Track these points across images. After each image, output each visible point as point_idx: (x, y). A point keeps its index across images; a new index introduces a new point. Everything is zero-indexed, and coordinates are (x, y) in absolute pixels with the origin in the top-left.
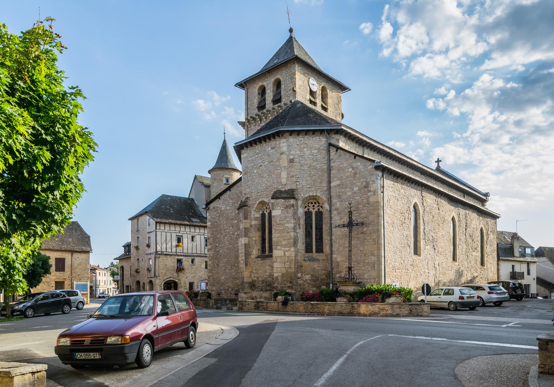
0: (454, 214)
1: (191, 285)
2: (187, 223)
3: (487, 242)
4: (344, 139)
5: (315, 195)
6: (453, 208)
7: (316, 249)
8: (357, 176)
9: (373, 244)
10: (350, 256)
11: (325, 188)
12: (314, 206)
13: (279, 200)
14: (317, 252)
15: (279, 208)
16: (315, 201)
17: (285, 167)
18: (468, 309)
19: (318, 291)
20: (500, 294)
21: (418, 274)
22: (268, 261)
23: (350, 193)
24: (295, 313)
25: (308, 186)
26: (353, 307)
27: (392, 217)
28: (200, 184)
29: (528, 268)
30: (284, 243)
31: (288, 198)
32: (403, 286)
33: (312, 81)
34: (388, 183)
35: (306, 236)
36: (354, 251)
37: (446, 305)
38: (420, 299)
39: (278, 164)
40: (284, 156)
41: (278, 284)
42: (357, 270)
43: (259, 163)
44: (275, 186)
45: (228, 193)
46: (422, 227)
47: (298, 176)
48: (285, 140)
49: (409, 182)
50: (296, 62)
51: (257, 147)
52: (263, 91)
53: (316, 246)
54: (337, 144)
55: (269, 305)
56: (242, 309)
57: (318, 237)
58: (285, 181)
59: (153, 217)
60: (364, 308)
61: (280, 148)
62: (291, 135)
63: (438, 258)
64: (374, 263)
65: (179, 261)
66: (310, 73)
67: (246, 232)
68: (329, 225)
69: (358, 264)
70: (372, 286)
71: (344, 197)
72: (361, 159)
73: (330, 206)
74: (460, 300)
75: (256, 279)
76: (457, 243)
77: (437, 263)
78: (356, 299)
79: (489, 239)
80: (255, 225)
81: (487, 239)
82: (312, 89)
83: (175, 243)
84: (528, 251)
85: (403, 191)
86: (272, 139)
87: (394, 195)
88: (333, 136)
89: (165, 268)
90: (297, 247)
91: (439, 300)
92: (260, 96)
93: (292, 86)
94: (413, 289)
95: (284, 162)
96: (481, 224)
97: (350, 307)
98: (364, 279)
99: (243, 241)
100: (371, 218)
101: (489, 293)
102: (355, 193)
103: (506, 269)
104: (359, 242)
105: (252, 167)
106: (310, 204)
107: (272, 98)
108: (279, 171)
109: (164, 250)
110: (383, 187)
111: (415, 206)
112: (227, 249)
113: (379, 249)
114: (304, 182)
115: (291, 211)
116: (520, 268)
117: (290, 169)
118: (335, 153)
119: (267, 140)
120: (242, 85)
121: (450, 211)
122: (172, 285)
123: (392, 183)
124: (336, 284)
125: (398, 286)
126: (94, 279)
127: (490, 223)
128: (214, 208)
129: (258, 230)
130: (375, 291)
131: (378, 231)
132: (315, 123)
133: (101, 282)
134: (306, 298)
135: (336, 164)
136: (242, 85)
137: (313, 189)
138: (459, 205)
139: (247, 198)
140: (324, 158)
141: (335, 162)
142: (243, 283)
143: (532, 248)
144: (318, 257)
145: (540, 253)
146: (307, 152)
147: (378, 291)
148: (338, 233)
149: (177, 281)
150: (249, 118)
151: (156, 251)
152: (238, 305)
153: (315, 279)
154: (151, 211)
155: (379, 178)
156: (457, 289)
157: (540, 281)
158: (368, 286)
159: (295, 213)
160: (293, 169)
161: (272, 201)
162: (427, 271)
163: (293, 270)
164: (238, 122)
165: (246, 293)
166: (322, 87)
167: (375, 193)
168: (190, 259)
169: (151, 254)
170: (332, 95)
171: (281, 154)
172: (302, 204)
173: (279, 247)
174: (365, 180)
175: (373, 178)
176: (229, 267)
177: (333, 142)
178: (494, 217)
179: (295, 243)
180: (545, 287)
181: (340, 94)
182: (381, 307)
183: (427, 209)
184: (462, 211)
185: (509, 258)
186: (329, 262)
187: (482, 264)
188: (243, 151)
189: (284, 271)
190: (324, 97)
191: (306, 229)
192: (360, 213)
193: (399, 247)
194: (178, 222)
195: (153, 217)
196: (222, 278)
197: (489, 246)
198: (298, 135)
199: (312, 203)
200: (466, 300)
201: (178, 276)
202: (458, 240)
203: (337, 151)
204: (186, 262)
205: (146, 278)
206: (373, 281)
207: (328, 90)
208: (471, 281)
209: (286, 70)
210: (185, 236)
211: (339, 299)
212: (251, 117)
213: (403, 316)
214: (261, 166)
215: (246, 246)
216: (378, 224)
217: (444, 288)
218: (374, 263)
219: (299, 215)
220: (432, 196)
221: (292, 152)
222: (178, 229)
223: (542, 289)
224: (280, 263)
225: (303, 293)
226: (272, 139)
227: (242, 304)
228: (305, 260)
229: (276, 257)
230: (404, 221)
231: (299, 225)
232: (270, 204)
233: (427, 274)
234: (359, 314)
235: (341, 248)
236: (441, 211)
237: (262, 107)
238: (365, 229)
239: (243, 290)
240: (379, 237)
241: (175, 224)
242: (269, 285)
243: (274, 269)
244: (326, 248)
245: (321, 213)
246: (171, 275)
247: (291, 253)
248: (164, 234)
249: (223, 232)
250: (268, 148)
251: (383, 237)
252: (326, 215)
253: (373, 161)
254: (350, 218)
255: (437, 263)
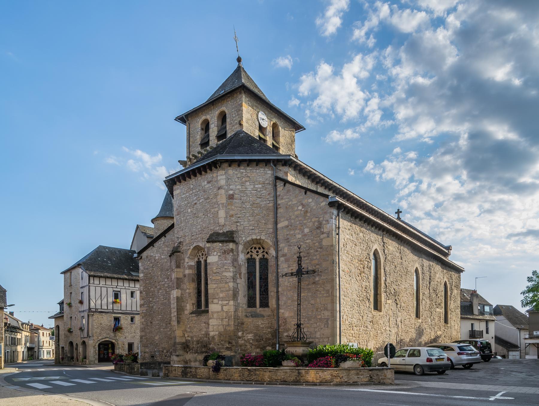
0: (417, 265)
1: (131, 346)
2: (126, 277)
3: (450, 297)
4: (293, 172)
5: (258, 238)
6: (416, 258)
7: (261, 303)
8: (308, 215)
9: (326, 297)
10: (299, 310)
11: (271, 230)
12: (257, 252)
13: (215, 244)
14: (261, 306)
15: (215, 253)
16: (260, 246)
17: (223, 204)
18: (436, 373)
19: (262, 353)
20: (471, 355)
21: (379, 332)
22: (203, 318)
23: (300, 236)
24: (228, 382)
25: (251, 228)
26: (299, 373)
27: (348, 264)
28: (142, 235)
29: (487, 326)
30: (221, 295)
31: (227, 241)
32: (362, 347)
33: (261, 115)
34: (344, 223)
35: (249, 288)
36: (304, 306)
37: (411, 369)
38: (380, 361)
39: (215, 200)
40: (222, 191)
41: (215, 344)
42: (308, 327)
43: (193, 201)
44: (212, 228)
45: (163, 239)
46: (383, 279)
47: (238, 216)
48: (224, 172)
49: (368, 224)
50: (243, 92)
51: (191, 182)
52: (206, 126)
53: (260, 300)
54: (285, 177)
55: (198, 371)
56: (168, 376)
57: (263, 289)
58: (222, 221)
59: (86, 270)
60: (312, 374)
61: (217, 181)
62: (230, 166)
63: (400, 314)
64: (328, 319)
65: (117, 319)
66: (259, 107)
67: (179, 283)
68: (275, 274)
69: (309, 320)
70: (325, 346)
71: (293, 241)
72: (313, 195)
73: (277, 251)
74: (428, 363)
75: (190, 339)
76: (421, 298)
77: (399, 319)
78: (306, 362)
79: (453, 294)
80: (189, 274)
81: (451, 294)
82: (262, 124)
83: (111, 299)
84: (487, 309)
85: (361, 234)
86: (208, 171)
87: (352, 239)
88: (281, 168)
89: (100, 329)
90: (237, 300)
91: (403, 362)
92: (204, 132)
93: (239, 120)
94: (372, 350)
95: (222, 199)
96: (445, 277)
97: (296, 373)
98: (315, 338)
99: (175, 293)
100: (324, 265)
101: (459, 354)
102: (305, 235)
103: (466, 326)
104: (310, 294)
105: (186, 205)
106: (253, 250)
107: (216, 133)
108: (216, 209)
109: (98, 307)
110: (339, 228)
111: (376, 254)
112: (162, 304)
113: (333, 302)
114: (246, 223)
115: (230, 256)
116: (480, 327)
117: (230, 207)
118: (282, 188)
119: (203, 173)
120: (183, 119)
121: (413, 261)
122: (110, 346)
123: (349, 224)
124: (283, 345)
125: (356, 346)
126: (36, 340)
127: (454, 278)
128: (147, 257)
129: (193, 281)
130: (328, 353)
131: (333, 280)
132: (260, 152)
133: (45, 342)
134: (247, 361)
135: (283, 201)
136: (183, 119)
137: (257, 231)
138: (423, 256)
139: (180, 243)
140: (269, 194)
141: (282, 199)
142: (175, 343)
143: (490, 306)
144: (263, 313)
145: (498, 311)
146: (249, 187)
147: (331, 352)
148: (286, 283)
149: (114, 341)
150: (191, 157)
151: (90, 309)
152: (164, 370)
153: (258, 339)
154: (84, 263)
155: (334, 217)
156: (424, 350)
157: (499, 340)
158: (320, 347)
159: (235, 260)
160: (233, 207)
161: (208, 245)
162: (388, 328)
163: (232, 328)
164: (179, 161)
165: (178, 356)
166: (274, 124)
167: (329, 234)
168: (129, 317)
169: (83, 311)
170: (284, 133)
171: (219, 189)
172: (243, 249)
173: (215, 301)
174: (317, 219)
175: (327, 217)
176: (164, 325)
177: (281, 175)
178: (459, 270)
179: (235, 296)
180: (502, 346)
181: (293, 134)
182: (335, 373)
183: (389, 258)
184: (426, 263)
185: (469, 316)
186: (275, 318)
187: (446, 321)
188: (175, 187)
189: (221, 329)
190: (275, 135)
191: (249, 279)
192: (311, 260)
193: (357, 301)
194: (115, 276)
195: (86, 270)
196: (156, 338)
197: (452, 302)
198: (239, 166)
199: (255, 248)
200: (434, 363)
201: (115, 336)
202: (421, 294)
203: (285, 185)
204: (125, 321)
205: (79, 338)
206: (325, 340)
207: (280, 128)
208: (435, 340)
209: (232, 101)
210: (123, 291)
211: (285, 363)
212: (193, 156)
213: (362, 385)
214: (196, 204)
215: (179, 299)
216: (333, 272)
217: (409, 348)
218: (328, 319)
219: (240, 262)
220: (394, 243)
221: (231, 187)
222: (115, 283)
223: (500, 348)
224: (217, 319)
225: (244, 355)
226: (208, 171)
227: (167, 369)
228: (246, 316)
229: (212, 312)
230: (362, 270)
231: (240, 274)
232: (206, 250)
233: (389, 332)
234: (308, 383)
235: (289, 301)
236: (404, 261)
237: (205, 144)
238: (317, 279)
239: (176, 352)
240: (333, 287)
241: (112, 278)
242: (205, 346)
243: (210, 326)
244: (272, 302)
245: (267, 260)
246: (108, 336)
247: (230, 307)
248: (98, 289)
249: (157, 284)
250: (204, 182)
251: (338, 287)
252: (272, 263)
253: (327, 196)
254: (300, 265)
255: (399, 319)
